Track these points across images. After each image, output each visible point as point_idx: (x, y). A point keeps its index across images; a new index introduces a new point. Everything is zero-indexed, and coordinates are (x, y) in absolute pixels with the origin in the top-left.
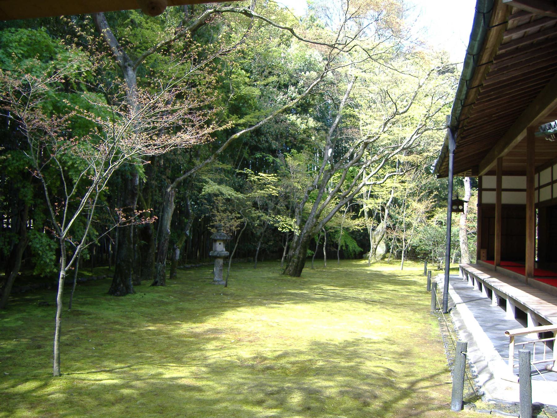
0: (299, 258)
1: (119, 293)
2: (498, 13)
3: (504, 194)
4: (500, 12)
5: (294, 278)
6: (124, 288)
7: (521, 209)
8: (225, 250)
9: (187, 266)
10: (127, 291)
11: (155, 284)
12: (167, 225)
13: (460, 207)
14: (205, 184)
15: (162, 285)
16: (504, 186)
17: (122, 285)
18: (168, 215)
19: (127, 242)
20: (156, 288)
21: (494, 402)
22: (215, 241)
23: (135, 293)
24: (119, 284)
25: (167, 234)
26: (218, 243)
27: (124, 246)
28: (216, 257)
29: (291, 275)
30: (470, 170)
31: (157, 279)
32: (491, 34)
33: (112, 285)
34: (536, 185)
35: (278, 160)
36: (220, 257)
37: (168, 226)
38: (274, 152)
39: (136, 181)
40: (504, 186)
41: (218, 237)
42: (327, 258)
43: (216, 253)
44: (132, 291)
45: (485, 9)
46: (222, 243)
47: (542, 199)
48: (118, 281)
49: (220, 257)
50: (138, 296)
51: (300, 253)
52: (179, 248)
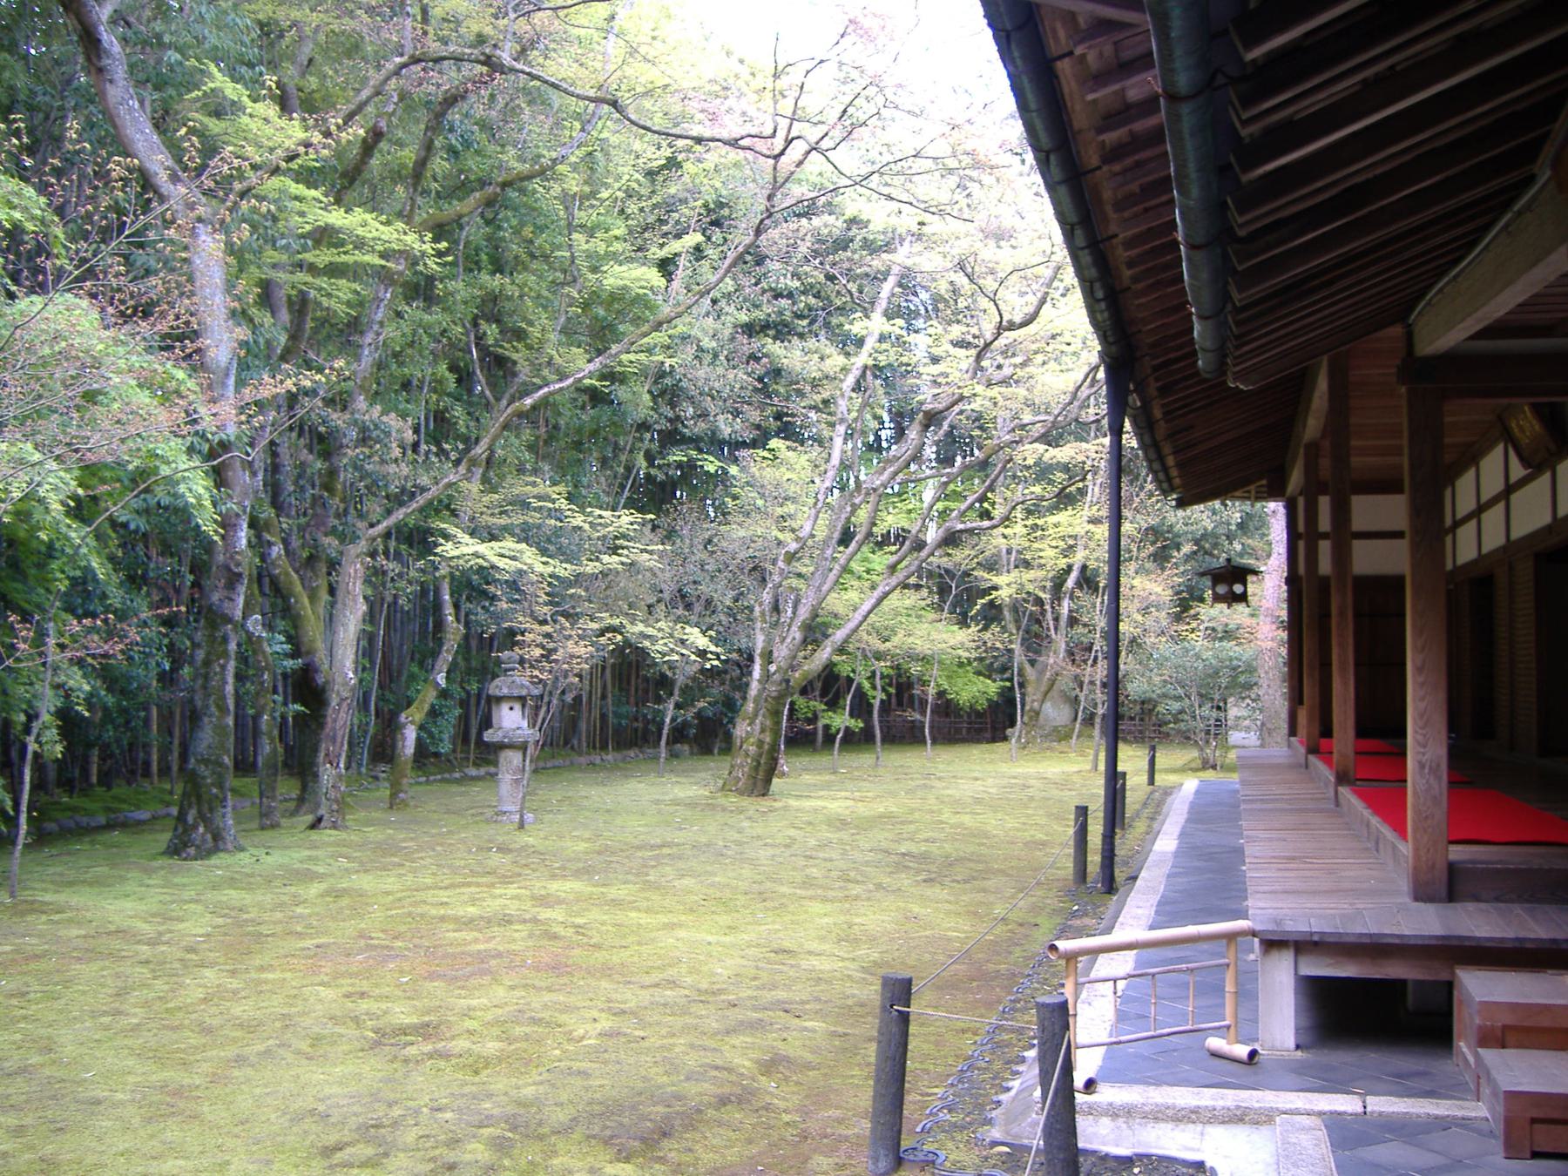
0: (760, 743)
1: (192, 851)
2: (1054, 31)
3: (1358, 546)
4: (1058, 25)
5: (746, 802)
6: (209, 836)
7: (1390, 587)
8: (525, 724)
9: (473, 771)
10: (217, 842)
11: (316, 825)
12: (344, 655)
13: (1238, 588)
14: (441, 541)
15: (335, 826)
16: (1358, 524)
17: (201, 829)
18: (346, 631)
19: (213, 709)
20: (314, 835)
21: (1006, 1149)
22: (499, 699)
23: (242, 849)
24: (195, 827)
25: (346, 684)
26: (505, 707)
27: (206, 720)
28: (502, 746)
29: (741, 793)
30: (1264, 482)
31: (322, 811)
32: (1066, 90)
33: (176, 829)
34: (1448, 521)
35: (733, 470)
36: (511, 746)
37: (349, 663)
38: (715, 444)
39: (239, 539)
40: (1358, 524)
41: (505, 691)
42: (884, 741)
43: (500, 733)
44: (230, 846)
45: (1005, 18)
46: (518, 707)
47: (1461, 561)
48: (190, 819)
49: (511, 746)
50: (244, 858)
51: (763, 731)
52: (412, 722)
